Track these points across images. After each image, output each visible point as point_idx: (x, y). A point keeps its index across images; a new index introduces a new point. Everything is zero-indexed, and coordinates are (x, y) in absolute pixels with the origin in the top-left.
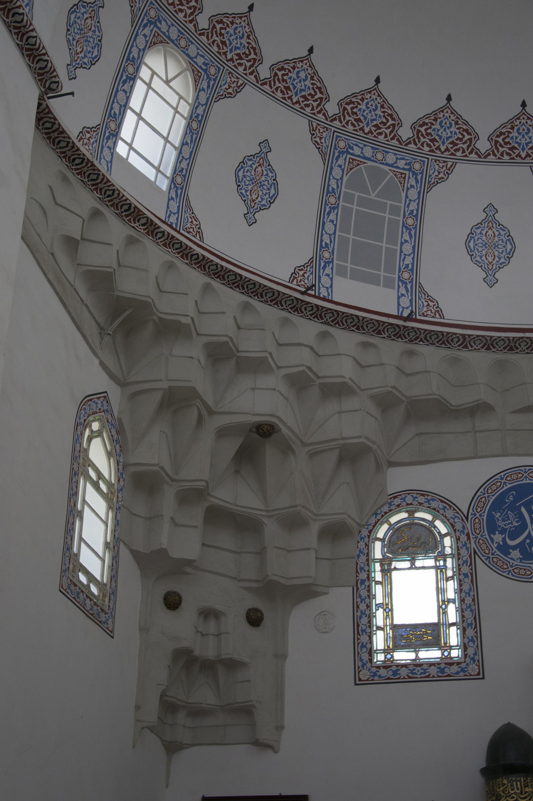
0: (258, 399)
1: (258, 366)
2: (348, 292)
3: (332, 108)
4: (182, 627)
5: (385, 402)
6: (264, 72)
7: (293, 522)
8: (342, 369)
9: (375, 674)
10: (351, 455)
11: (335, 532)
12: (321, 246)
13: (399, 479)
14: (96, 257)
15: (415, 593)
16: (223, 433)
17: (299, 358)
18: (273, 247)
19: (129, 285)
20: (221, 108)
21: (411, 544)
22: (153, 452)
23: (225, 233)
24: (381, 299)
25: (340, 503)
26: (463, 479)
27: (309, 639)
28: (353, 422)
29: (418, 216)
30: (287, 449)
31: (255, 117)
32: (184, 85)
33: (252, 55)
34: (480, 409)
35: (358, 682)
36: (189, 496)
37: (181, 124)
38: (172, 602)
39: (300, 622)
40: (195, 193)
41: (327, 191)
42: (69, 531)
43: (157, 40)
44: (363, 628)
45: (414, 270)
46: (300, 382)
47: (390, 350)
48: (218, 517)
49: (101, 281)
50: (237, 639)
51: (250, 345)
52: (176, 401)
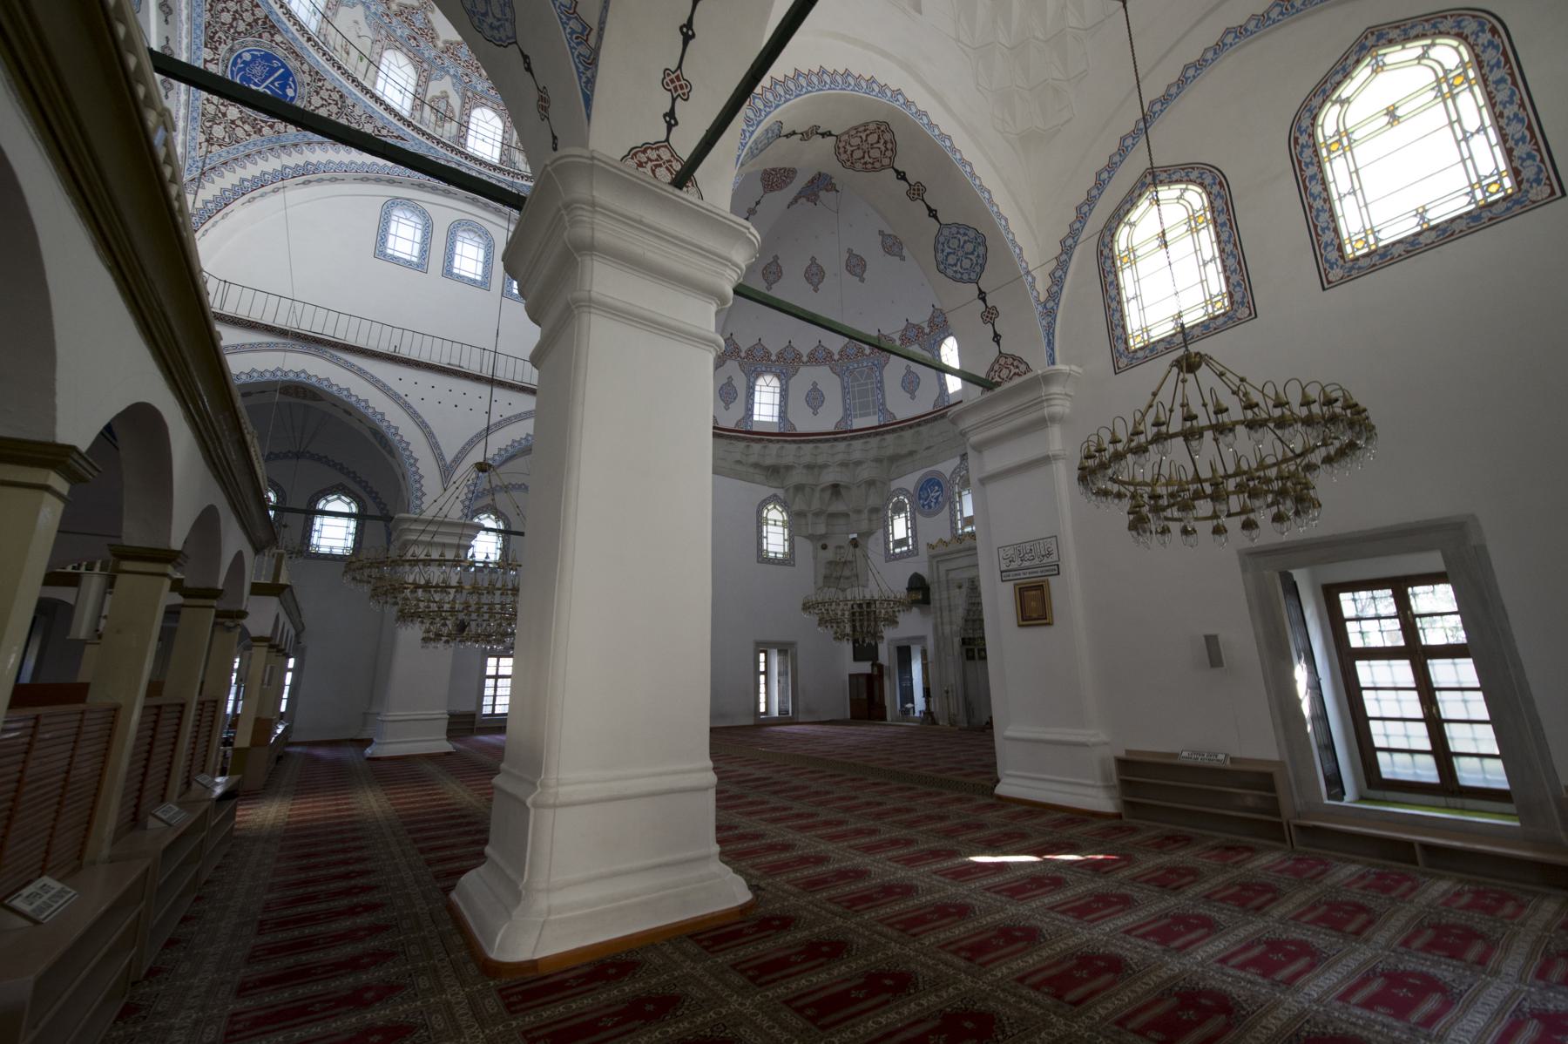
0: (829, 477)
1: (824, 466)
2: (858, 423)
3: (836, 357)
4: (829, 554)
5: (878, 460)
6: (805, 359)
7: (859, 512)
8: (857, 455)
9: (1352, 268)
10: (871, 483)
11: (875, 510)
12: (845, 410)
13: (895, 485)
14: (753, 459)
15: (900, 528)
16: (823, 490)
17: (840, 457)
18: (826, 421)
19: (768, 461)
20: (792, 381)
21: (899, 509)
22: (799, 505)
23: (805, 422)
24: (872, 421)
25: (874, 500)
26: (910, 481)
27: (874, 547)
28: (865, 473)
29: (881, 382)
30: (847, 488)
31: (923, 404)
32: (776, 382)
33: (798, 356)
34: (911, 453)
35: (1326, 284)
36: (817, 514)
37: (777, 396)
38: (824, 547)
39: (872, 540)
40: (790, 416)
41: (844, 388)
42: (760, 544)
43: (759, 374)
44: (887, 543)
45: (883, 404)
46: (844, 464)
47: (874, 441)
48: (832, 516)
49: (756, 465)
50: (848, 554)
51: (820, 460)
52: (799, 488)
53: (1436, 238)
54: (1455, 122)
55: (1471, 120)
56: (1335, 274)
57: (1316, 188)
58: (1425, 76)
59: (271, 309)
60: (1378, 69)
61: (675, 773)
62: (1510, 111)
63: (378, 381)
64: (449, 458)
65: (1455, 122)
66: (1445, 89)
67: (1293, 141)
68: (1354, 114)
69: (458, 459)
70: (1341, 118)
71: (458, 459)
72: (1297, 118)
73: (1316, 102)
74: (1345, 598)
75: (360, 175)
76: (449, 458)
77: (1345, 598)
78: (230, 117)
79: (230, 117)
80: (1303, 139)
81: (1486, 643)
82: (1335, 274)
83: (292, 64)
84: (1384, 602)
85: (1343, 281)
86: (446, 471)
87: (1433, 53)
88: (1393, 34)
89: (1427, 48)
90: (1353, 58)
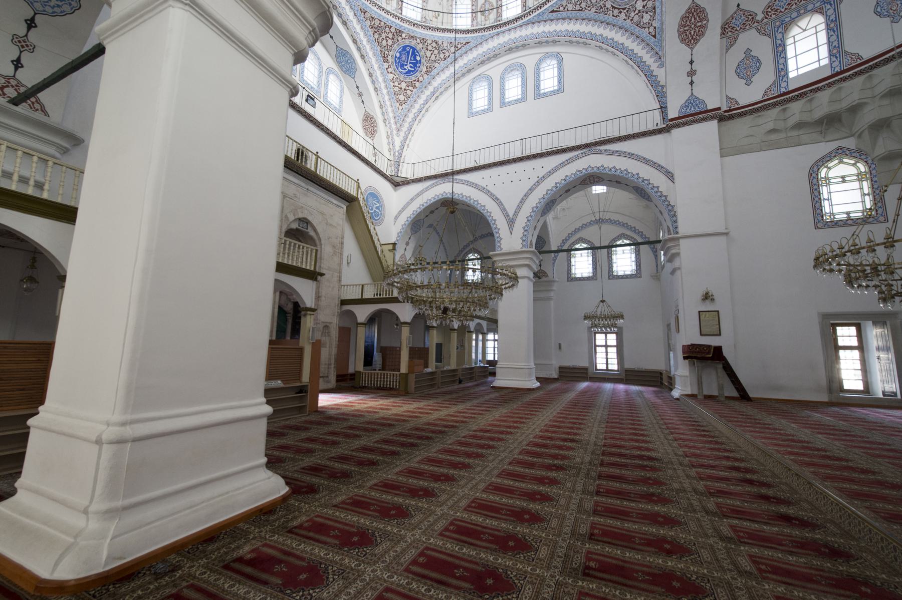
35: (816, 228)
53: (849, 222)
54: (861, 189)
55: (866, 191)
56: (820, 225)
57: (816, 193)
58: (854, 171)
59: (616, 129)
60: (841, 162)
61: (231, 408)
62: (877, 192)
63: (556, 167)
64: (511, 215)
65: (861, 189)
66: (860, 177)
67: (810, 175)
68: (831, 174)
69: (516, 214)
70: (827, 173)
71: (516, 214)
72: (812, 167)
73: (820, 164)
74: (838, 328)
75: (568, 39)
76: (511, 215)
77: (838, 328)
78: (641, 8)
79: (641, 8)
80: (814, 175)
81: (620, 347)
82: (820, 225)
83: (413, 43)
84: (853, 330)
85: (822, 228)
86: (511, 223)
87: (858, 164)
88: (848, 152)
89: (857, 162)
90: (833, 154)
